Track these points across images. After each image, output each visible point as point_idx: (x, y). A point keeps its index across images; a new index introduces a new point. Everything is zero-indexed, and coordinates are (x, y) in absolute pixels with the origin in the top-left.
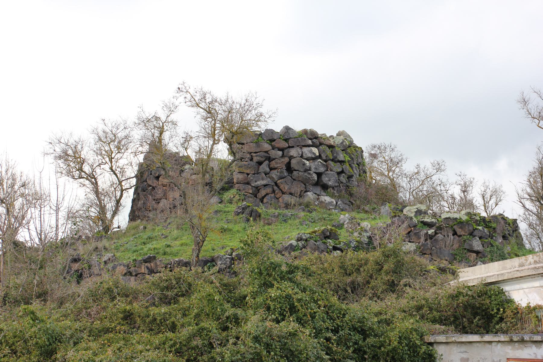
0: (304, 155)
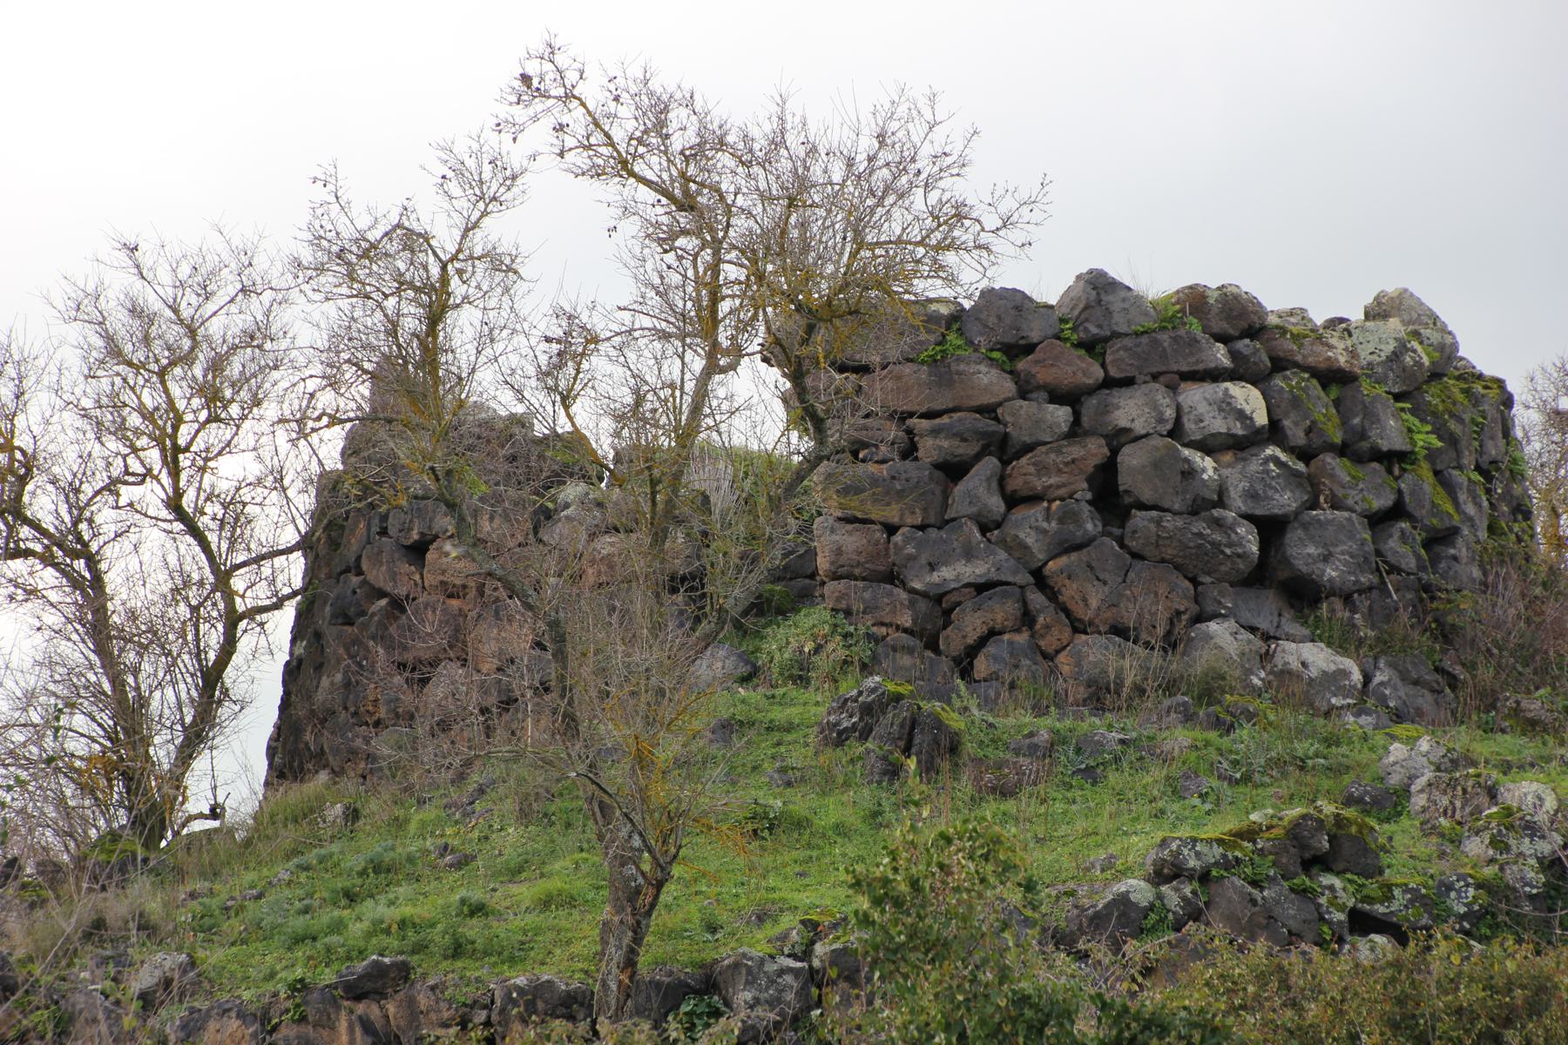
0: (1189, 425)
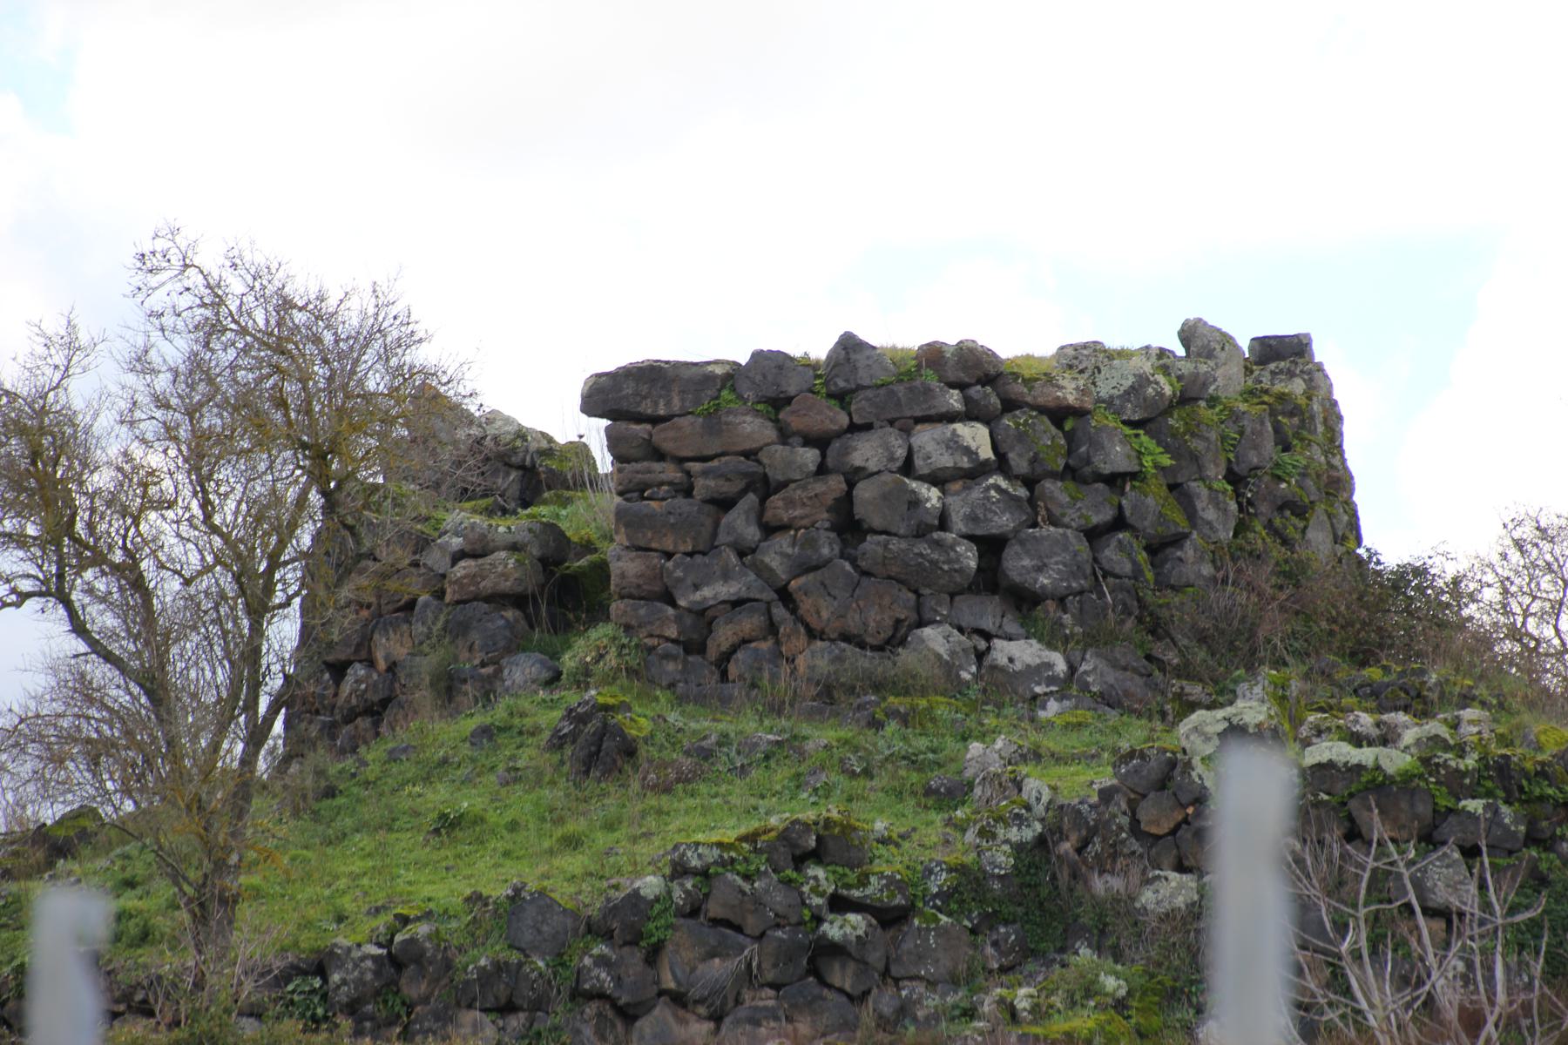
0: (918, 462)
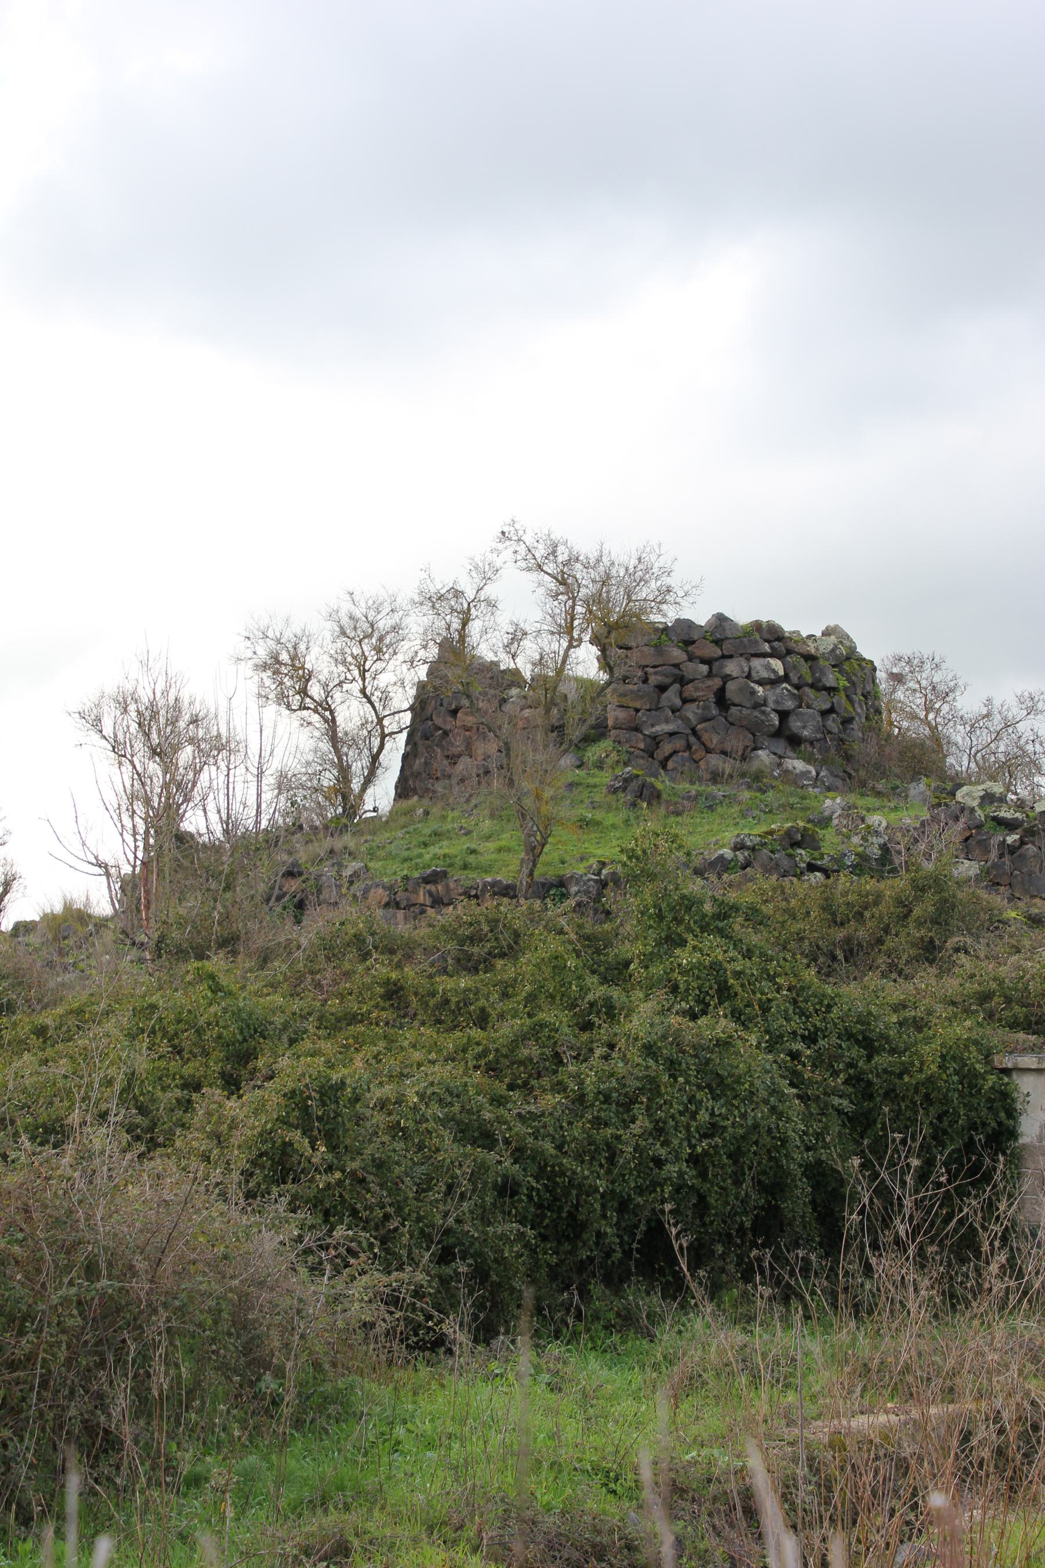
0: (754, 674)
